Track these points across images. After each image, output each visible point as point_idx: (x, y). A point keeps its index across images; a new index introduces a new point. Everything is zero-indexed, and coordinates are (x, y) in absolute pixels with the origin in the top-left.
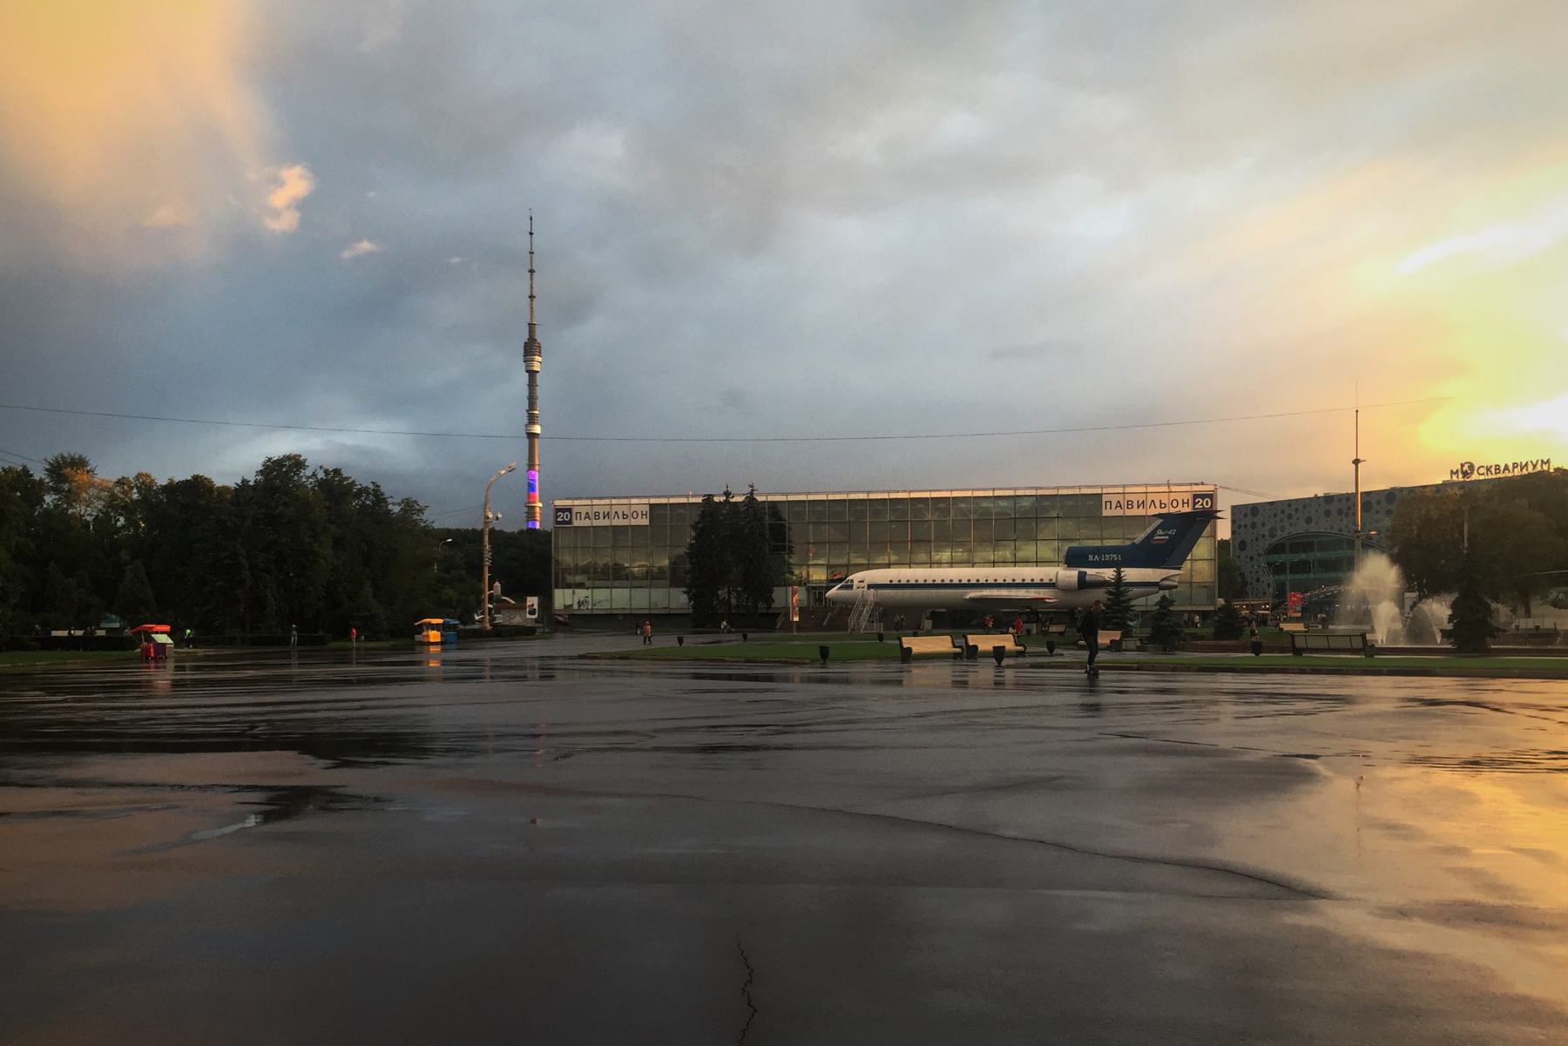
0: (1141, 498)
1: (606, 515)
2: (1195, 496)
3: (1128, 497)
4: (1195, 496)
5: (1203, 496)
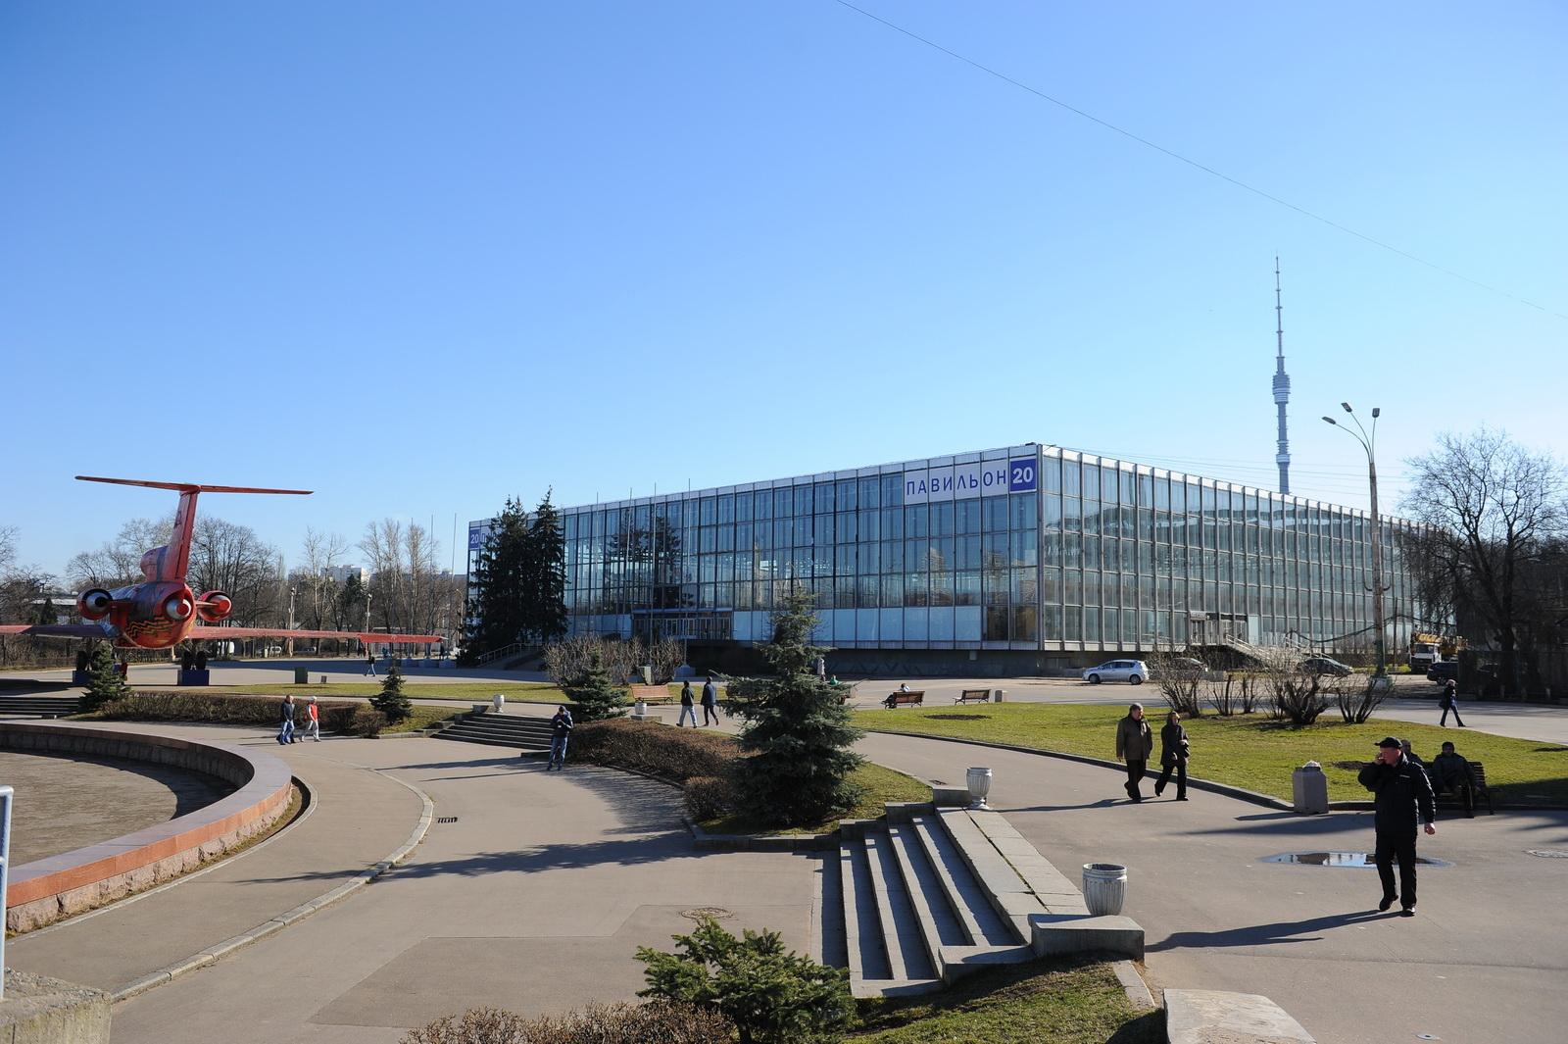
0: (948, 473)
1: (949, 483)
2: (1014, 465)
3: (934, 474)
4: (1014, 465)
5: (1022, 465)
